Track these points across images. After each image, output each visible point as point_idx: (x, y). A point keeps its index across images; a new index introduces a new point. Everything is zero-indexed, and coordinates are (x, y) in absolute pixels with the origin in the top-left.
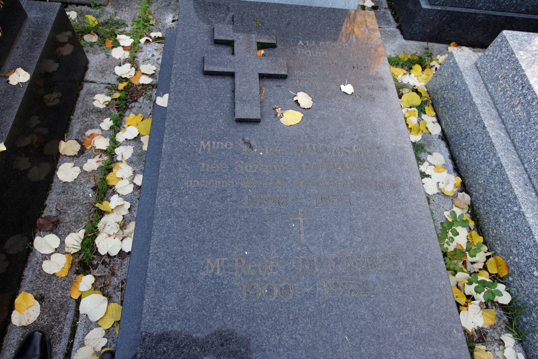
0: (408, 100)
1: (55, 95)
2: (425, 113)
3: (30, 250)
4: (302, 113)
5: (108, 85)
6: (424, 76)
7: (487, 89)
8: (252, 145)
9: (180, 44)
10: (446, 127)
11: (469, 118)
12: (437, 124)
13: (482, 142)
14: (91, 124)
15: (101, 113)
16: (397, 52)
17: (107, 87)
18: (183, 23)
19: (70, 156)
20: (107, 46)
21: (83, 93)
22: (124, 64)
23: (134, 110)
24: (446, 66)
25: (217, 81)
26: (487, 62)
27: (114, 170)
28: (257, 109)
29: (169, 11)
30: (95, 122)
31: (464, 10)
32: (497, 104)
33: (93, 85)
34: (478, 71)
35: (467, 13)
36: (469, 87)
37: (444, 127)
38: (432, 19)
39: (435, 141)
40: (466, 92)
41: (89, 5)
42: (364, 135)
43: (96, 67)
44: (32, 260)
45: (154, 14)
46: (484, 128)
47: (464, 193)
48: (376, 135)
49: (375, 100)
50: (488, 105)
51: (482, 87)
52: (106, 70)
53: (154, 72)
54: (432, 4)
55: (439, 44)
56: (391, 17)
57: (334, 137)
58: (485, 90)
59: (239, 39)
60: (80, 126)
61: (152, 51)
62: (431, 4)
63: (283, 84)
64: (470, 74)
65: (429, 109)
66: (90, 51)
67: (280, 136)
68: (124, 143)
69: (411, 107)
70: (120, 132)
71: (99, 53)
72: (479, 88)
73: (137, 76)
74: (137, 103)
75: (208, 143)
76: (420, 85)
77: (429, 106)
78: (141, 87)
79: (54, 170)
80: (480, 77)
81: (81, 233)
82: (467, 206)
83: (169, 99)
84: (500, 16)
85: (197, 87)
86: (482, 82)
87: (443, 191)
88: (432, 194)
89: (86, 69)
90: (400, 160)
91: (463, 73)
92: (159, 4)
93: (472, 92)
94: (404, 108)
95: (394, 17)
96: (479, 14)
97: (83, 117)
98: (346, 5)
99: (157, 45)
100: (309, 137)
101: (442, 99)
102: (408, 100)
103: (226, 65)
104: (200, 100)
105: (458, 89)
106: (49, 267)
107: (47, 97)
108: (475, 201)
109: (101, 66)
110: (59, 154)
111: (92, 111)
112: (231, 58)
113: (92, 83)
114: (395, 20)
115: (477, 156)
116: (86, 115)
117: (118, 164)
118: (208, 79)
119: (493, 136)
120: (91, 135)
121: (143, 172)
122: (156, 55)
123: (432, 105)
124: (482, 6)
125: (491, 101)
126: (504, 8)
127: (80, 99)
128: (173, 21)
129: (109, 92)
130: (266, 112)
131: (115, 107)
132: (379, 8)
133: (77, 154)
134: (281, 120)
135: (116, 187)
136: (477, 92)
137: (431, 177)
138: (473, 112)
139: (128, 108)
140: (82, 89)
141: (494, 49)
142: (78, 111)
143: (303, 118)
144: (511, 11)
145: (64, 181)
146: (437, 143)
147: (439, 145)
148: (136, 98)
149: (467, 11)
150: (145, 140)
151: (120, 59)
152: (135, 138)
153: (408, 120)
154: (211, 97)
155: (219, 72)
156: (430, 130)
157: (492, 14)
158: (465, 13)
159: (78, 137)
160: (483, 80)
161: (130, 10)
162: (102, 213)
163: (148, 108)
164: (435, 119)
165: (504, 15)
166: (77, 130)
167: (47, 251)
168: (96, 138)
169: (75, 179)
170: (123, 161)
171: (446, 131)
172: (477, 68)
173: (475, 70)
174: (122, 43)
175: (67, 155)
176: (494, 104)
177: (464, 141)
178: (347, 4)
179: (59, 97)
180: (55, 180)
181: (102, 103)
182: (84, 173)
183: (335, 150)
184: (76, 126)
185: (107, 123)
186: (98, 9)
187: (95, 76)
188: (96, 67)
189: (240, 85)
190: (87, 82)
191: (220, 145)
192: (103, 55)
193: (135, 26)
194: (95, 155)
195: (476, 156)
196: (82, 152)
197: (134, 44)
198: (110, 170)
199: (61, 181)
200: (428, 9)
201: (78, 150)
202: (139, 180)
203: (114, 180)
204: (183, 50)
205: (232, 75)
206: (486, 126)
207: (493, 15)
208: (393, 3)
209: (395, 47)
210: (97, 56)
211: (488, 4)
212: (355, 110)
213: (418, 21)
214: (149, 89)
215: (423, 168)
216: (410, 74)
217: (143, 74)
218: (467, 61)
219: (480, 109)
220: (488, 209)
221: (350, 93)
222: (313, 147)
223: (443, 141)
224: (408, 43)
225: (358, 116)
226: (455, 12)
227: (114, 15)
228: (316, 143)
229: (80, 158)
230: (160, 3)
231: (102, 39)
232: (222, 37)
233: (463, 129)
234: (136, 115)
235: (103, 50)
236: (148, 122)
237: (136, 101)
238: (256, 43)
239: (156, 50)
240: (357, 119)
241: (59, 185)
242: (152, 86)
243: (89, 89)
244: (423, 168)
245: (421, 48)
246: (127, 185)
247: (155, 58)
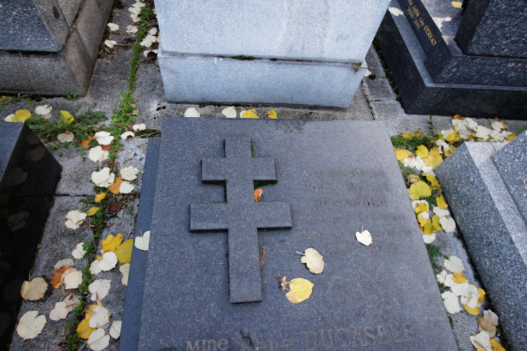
0: (417, 191)
2: (436, 205)
4: (312, 282)
5: (84, 198)
6: (431, 158)
7: (509, 191)
8: (253, 341)
9: (161, 187)
10: (461, 224)
11: (491, 225)
12: (451, 219)
13: (509, 258)
14: (62, 253)
16: (400, 129)
17: (81, 201)
18: (165, 157)
19: (34, 301)
20: (83, 146)
21: (53, 210)
22: (102, 168)
23: (113, 229)
24: (458, 156)
25: (206, 241)
26: (506, 160)
27: (87, 316)
28: (257, 286)
29: (153, 97)
30: (67, 249)
31: (469, 87)
32: (522, 211)
33: (65, 199)
34: (496, 167)
35: (473, 89)
36: (489, 188)
37: (459, 224)
38: (435, 96)
39: (451, 241)
40: (485, 193)
41: (65, 97)
42: (389, 307)
43: (70, 175)
45: (137, 101)
46: (512, 242)
47: (490, 311)
48: (404, 306)
49: (398, 251)
50: (512, 212)
51: (502, 188)
52: (82, 177)
53: (135, 177)
54: (437, 82)
55: (442, 117)
56: (390, 88)
57: (354, 314)
58: (506, 191)
59: (233, 178)
60: (48, 257)
61: (134, 148)
62: (434, 82)
63: (287, 237)
64: (487, 172)
65: (440, 200)
66: (64, 153)
67: (287, 322)
68: (100, 276)
69: (420, 199)
70: (96, 261)
71: (75, 156)
72: (500, 190)
73: (117, 183)
74: (116, 219)
75: (197, 343)
76: (428, 170)
77: (440, 196)
78: (121, 197)
79: (14, 322)
80: (499, 174)
82: (495, 328)
83: (151, 234)
84: (507, 91)
85: (182, 253)
86: (502, 181)
87: (466, 309)
88: (454, 313)
89: (59, 178)
90: (436, 344)
91: (480, 171)
92: (143, 89)
93: (492, 196)
94: (413, 200)
95: (393, 87)
96: (485, 90)
97: (52, 244)
98: (345, 88)
99: (140, 139)
100: (323, 318)
101: (455, 191)
102: (417, 191)
103: (218, 219)
104: (186, 273)
105: (474, 187)
107: (11, 219)
108: (504, 322)
109: (76, 173)
110: (20, 300)
111: (63, 235)
112: (223, 206)
113: (65, 197)
114: (394, 91)
115: (504, 271)
116: (56, 240)
117: (92, 306)
118: (196, 238)
119: (523, 254)
120: (61, 268)
121: (121, 316)
122: (138, 154)
123: (443, 193)
124: (488, 82)
125: (515, 206)
126: (511, 83)
127: (50, 219)
128: (158, 109)
129: (84, 207)
130: (268, 285)
131: (91, 227)
132: (377, 77)
133: (43, 298)
134: (287, 295)
135: (89, 342)
136: (498, 195)
137: (451, 290)
138: (496, 219)
139: (106, 226)
140: (52, 205)
141: (516, 149)
142: (47, 237)
143: (313, 289)
144: (518, 85)
145: (25, 339)
146: (453, 243)
147: (455, 245)
148: (115, 214)
149: (472, 88)
150: (125, 269)
151: (98, 161)
152: (113, 269)
153: (419, 216)
154: (199, 268)
155: (209, 230)
156: (444, 227)
157: (499, 89)
158: (470, 89)
159: (46, 272)
160: (502, 178)
161: (111, 99)
163: (129, 225)
164: (447, 213)
165: (511, 89)
166: (45, 263)
168: (67, 271)
169: (39, 334)
170: (99, 302)
171: (462, 229)
172: (494, 163)
173: (492, 165)
174: (100, 142)
175: (31, 299)
176: (519, 210)
177: (486, 248)
178: (346, 86)
179: (26, 218)
180: (14, 339)
181: (76, 223)
182: (50, 323)
183: (356, 337)
186: (75, 100)
187: (69, 187)
188: (70, 175)
189: (235, 248)
190: (60, 195)
191: (212, 345)
192: (78, 159)
193: (115, 120)
194: (65, 297)
195: (502, 272)
196: (49, 293)
197: (114, 142)
199: (22, 338)
200: (432, 88)
201: (44, 292)
202: (116, 330)
203: (86, 330)
204: (165, 197)
205: (222, 183)
206: (514, 240)
207: (499, 90)
208: (391, 73)
209: (397, 124)
210: (71, 160)
211: (494, 81)
212: (376, 269)
213: (421, 98)
214: (130, 199)
215: (442, 278)
216: (416, 156)
217: (124, 180)
218: (482, 155)
219: (505, 218)
220: (522, 339)
221: (367, 244)
222: (328, 334)
223: (459, 240)
224: (410, 118)
225: (380, 278)
226: (460, 89)
227: (93, 106)
228: (332, 328)
229: (47, 302)
230: (145, 87)
231: (78, 141)
232: (211, 177)
233: (484, 235)
234: (115, 235)
235: (79, 152)
237: (115, 216)
238: (252, 182)
239: (139, 147)
240: (379, 283)
241: (19, 344)
242: (133, 195)
243: (61, 205)
244: (442, 278)
245: (424, 122)
246: (101, 338)
247: (138, 158)
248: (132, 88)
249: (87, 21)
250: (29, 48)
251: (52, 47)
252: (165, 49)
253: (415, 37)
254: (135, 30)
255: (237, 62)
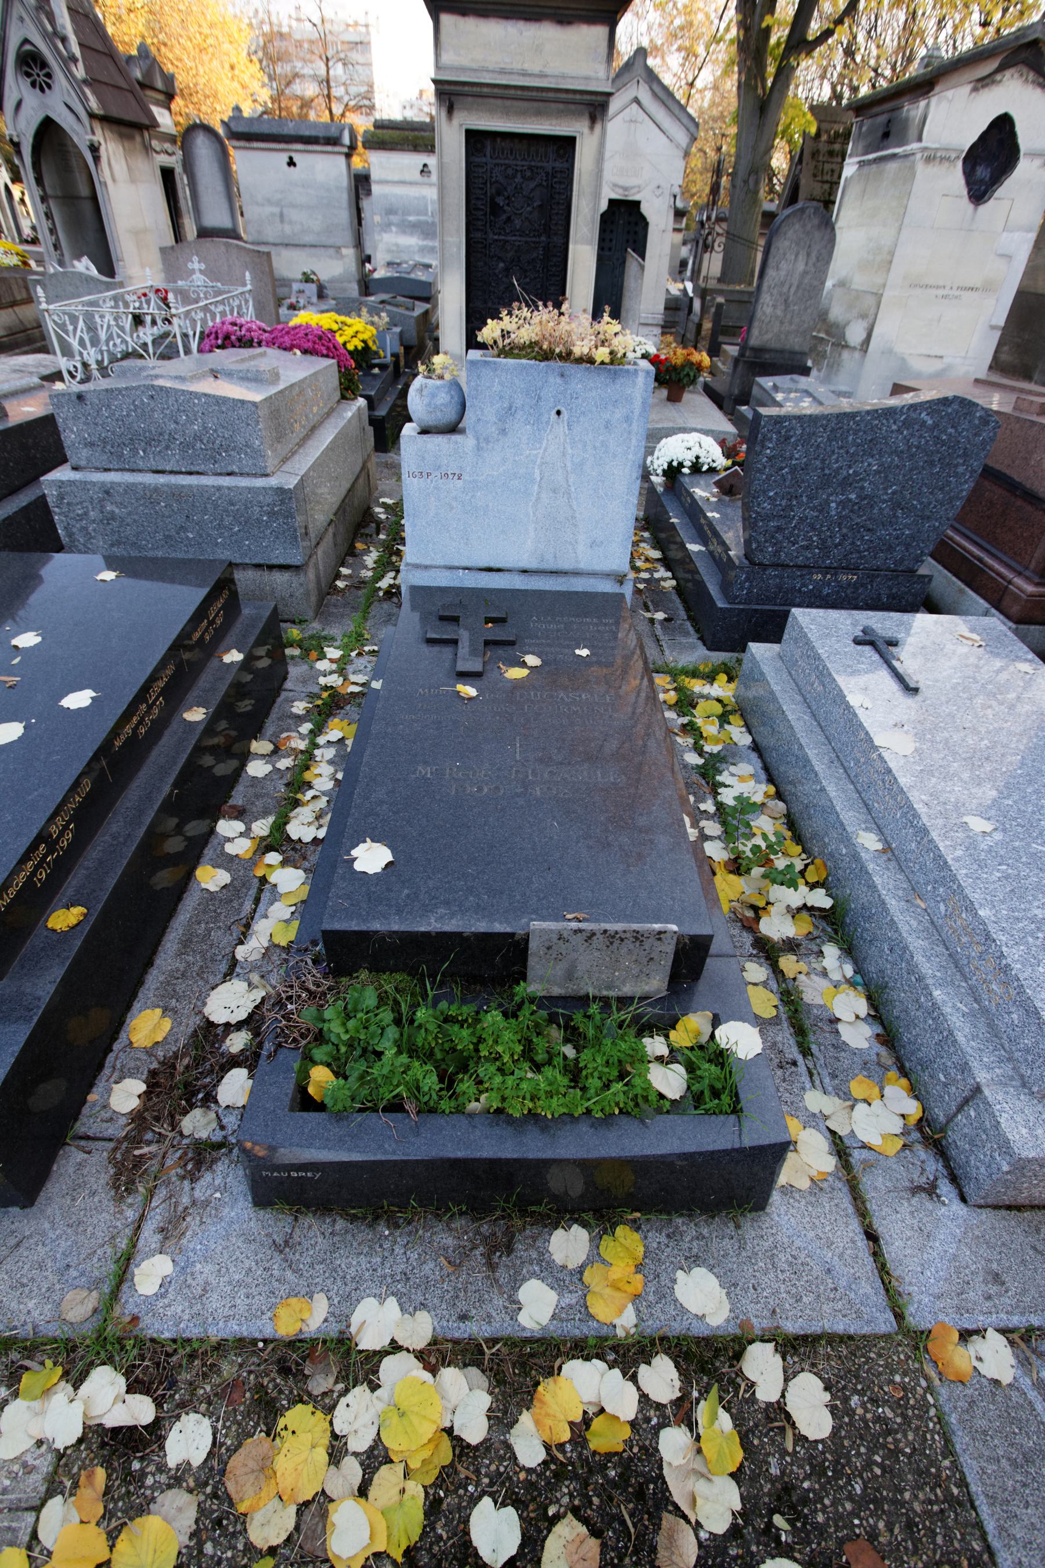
1: (247, 702)
3: (212, 831)
15: (300, 719)
21: (279, 700)
44: (214, 841)
79: (243, 766)
81: (271, 819)
89: (285, 679)
106: (230, 849)
127: (276, 705)
150: (349, 742)
162: (296, 803)
167: (231, 835)
180: (243, 775)
184: (270, 728)
185: (306, 727)
192: (305, 667)
197: (343, 656)
198: (308, 768)
231: (306, 652)
236: (354, 727)
248: (365, 619)
249: (324, 552)
250: (275, 562)
251: (297, 560)
252: (409, 561)
253: (715, 569)
254: (370, 574)
255: (484, 574)
